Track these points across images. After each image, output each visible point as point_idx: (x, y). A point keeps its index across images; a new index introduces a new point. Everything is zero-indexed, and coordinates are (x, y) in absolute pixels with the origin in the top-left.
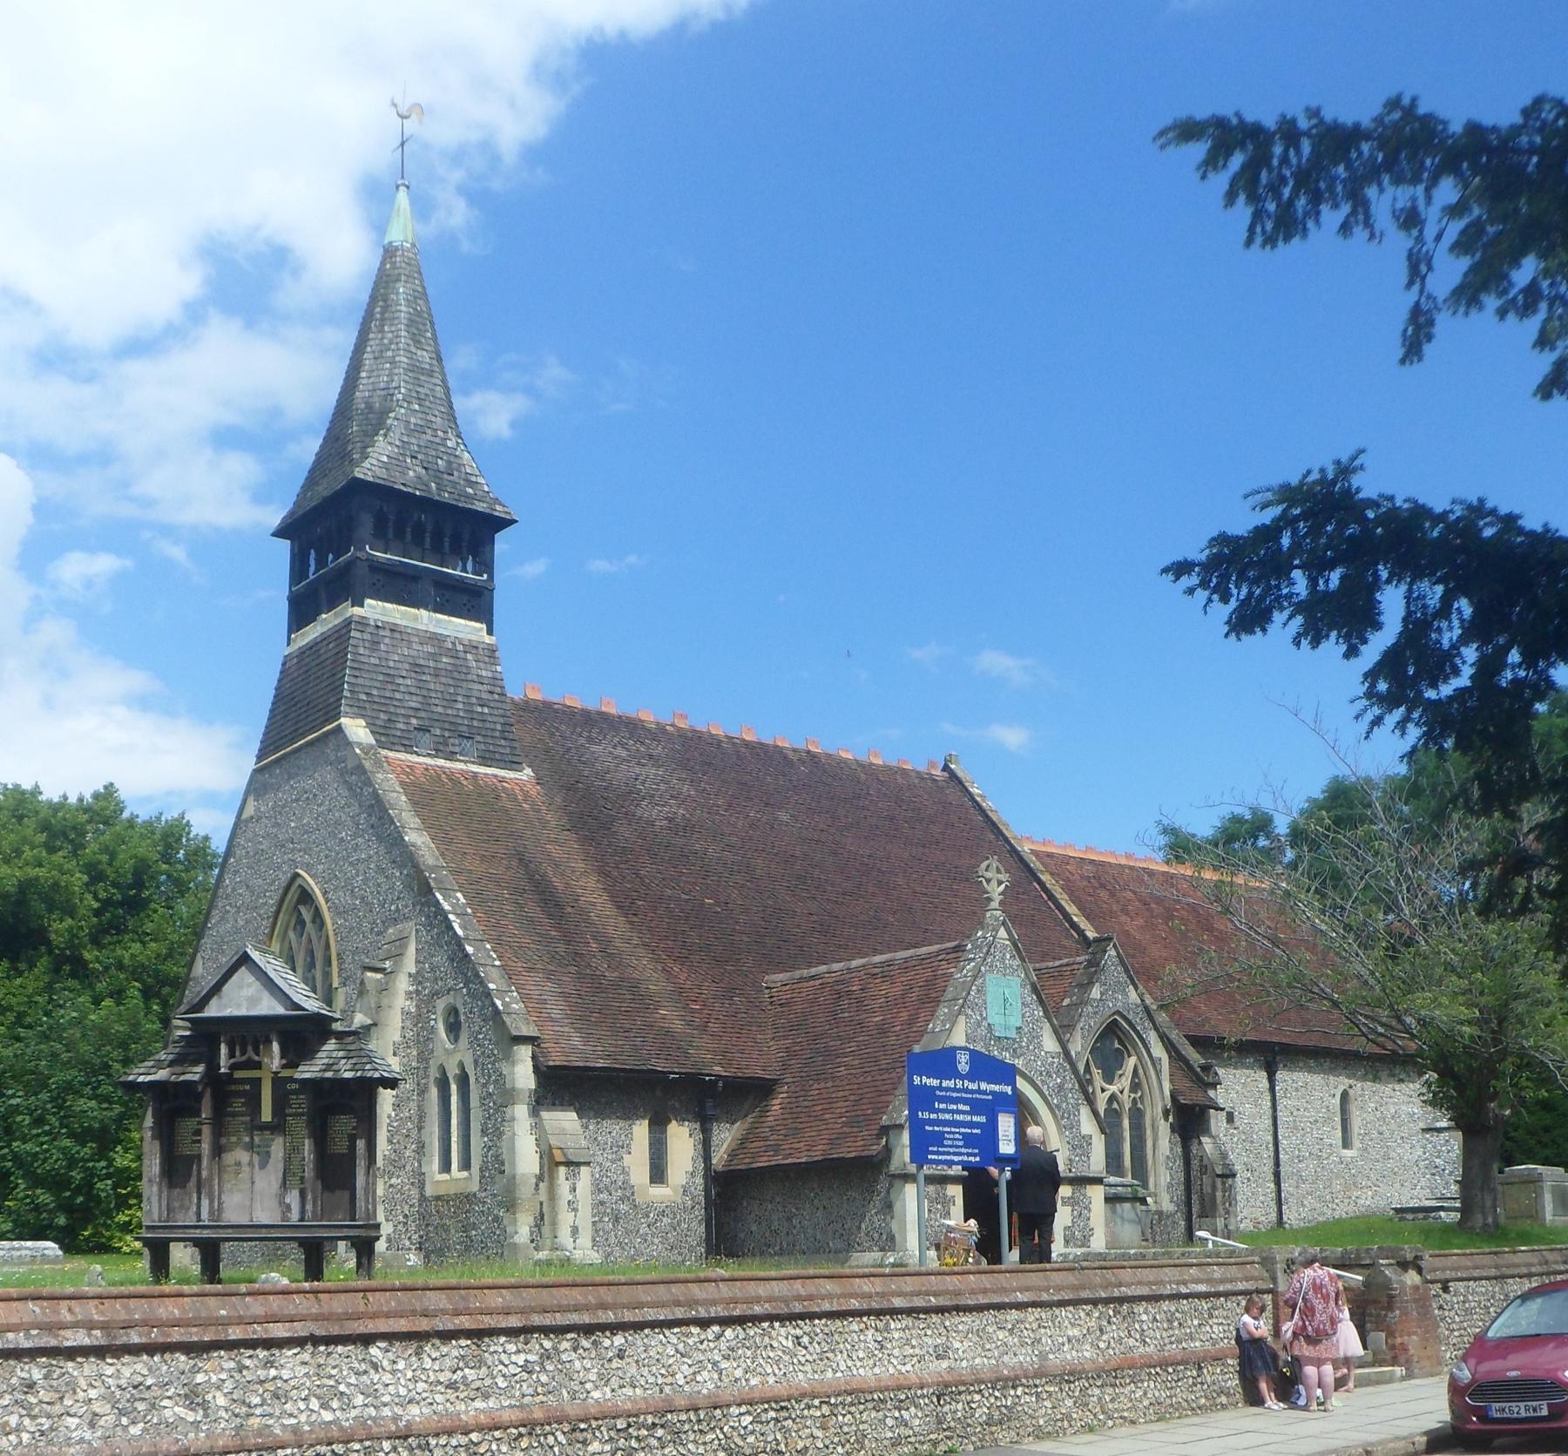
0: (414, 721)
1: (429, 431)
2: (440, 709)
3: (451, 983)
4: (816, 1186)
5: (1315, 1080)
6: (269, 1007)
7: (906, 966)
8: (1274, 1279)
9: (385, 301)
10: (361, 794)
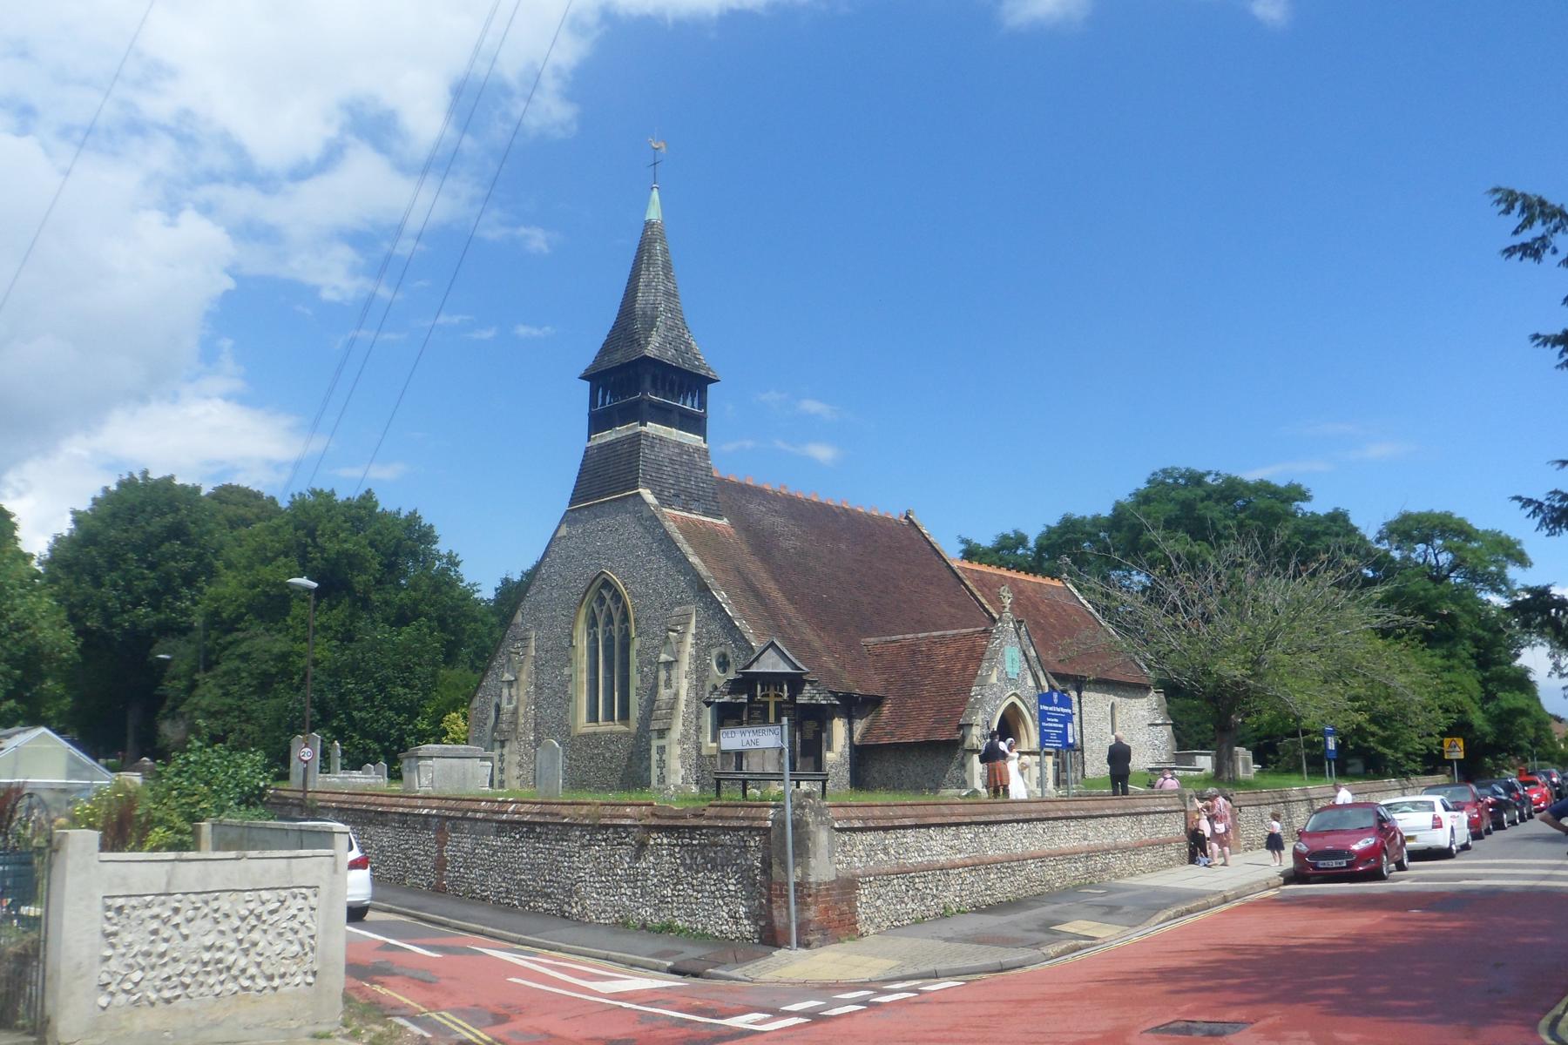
2: (683, 485)
5: (1099, 696)
7: (954, 638)
8: (1185, 805)
10: (654, 533)
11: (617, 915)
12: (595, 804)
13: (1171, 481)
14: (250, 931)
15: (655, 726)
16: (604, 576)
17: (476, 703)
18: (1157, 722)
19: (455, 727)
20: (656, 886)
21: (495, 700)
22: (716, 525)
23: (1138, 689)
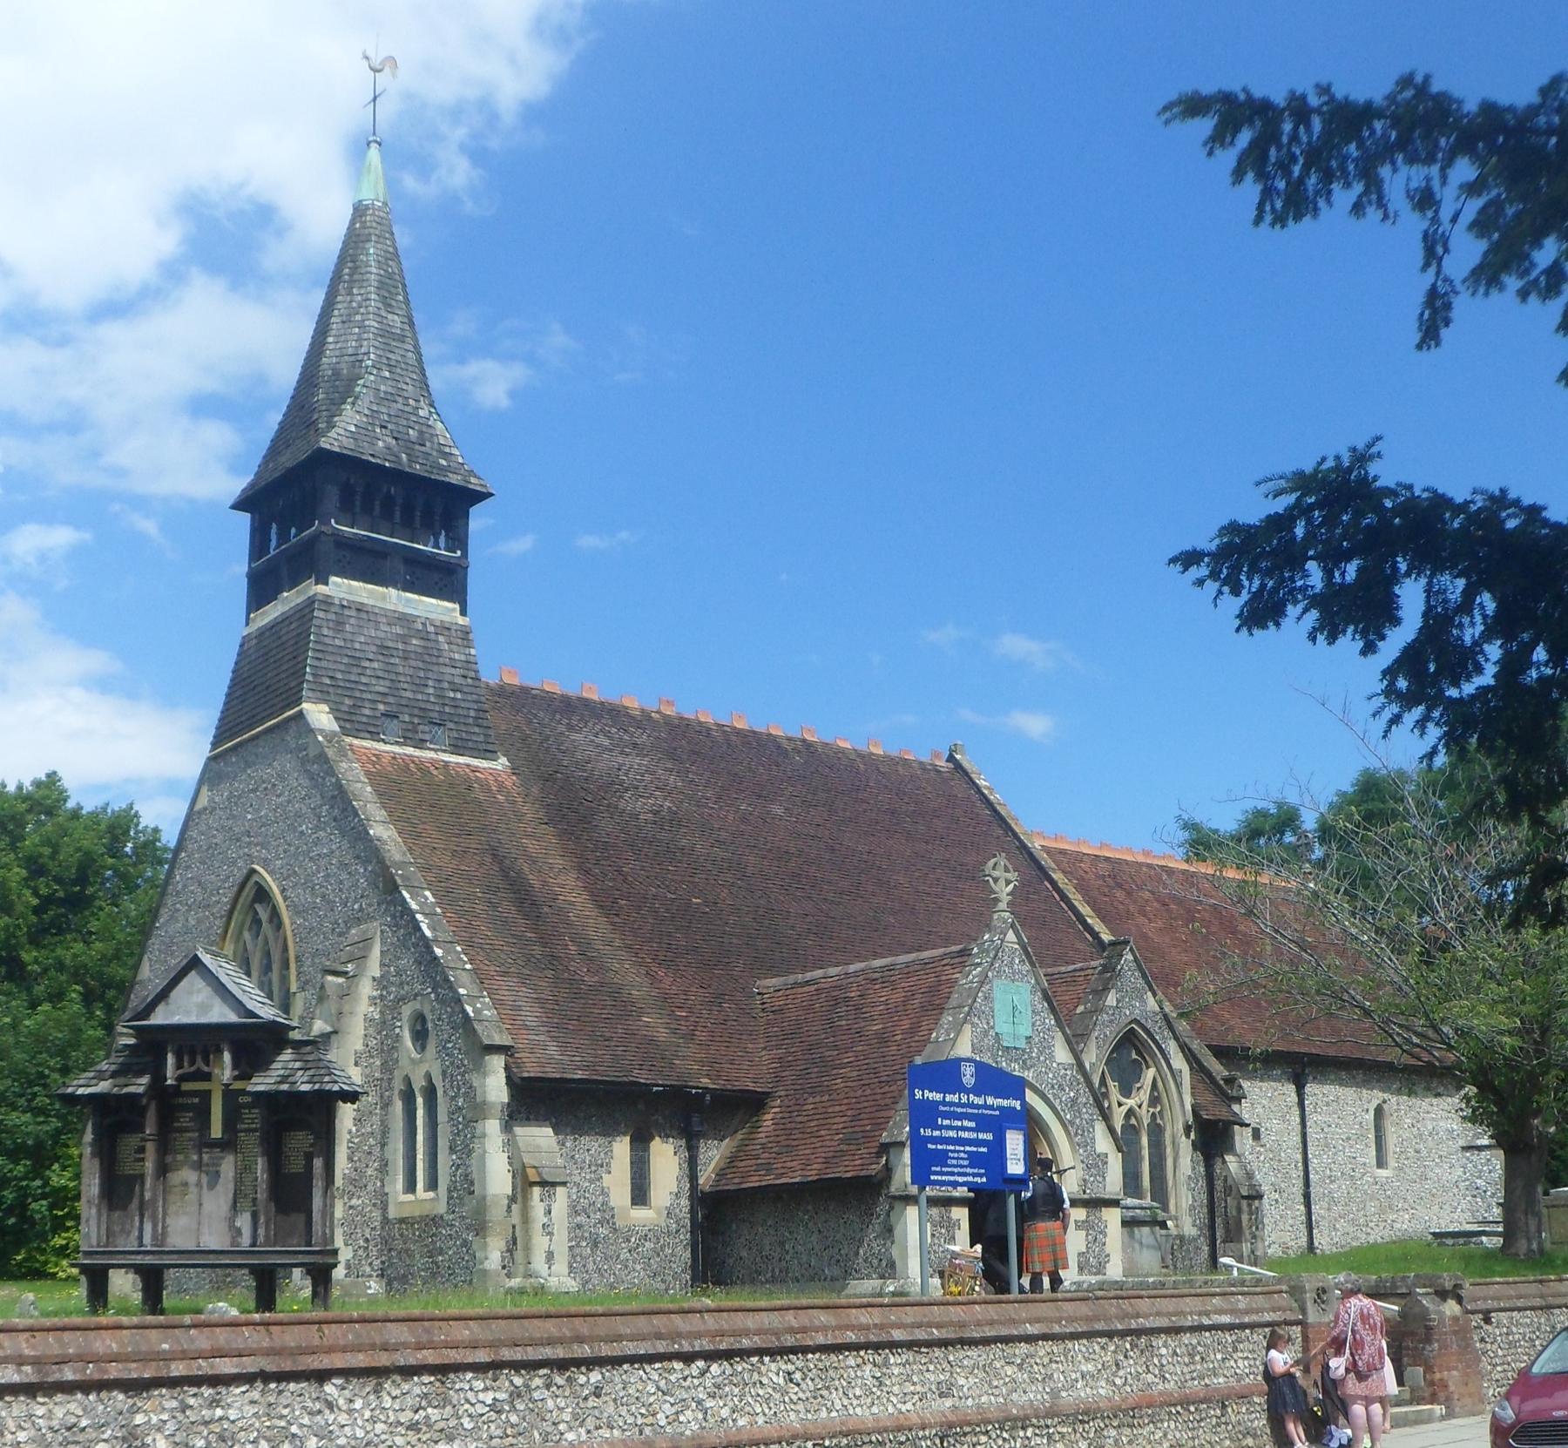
0: (381, 707)
1: (400, 400)
2: (409, 694)
4: (810, 1208)
5: (1348, 1094)
6: (221, 1014)
7: (908, 971)
8: (1303, 1310)
18: (1479, 1142)
22: (475, 770)
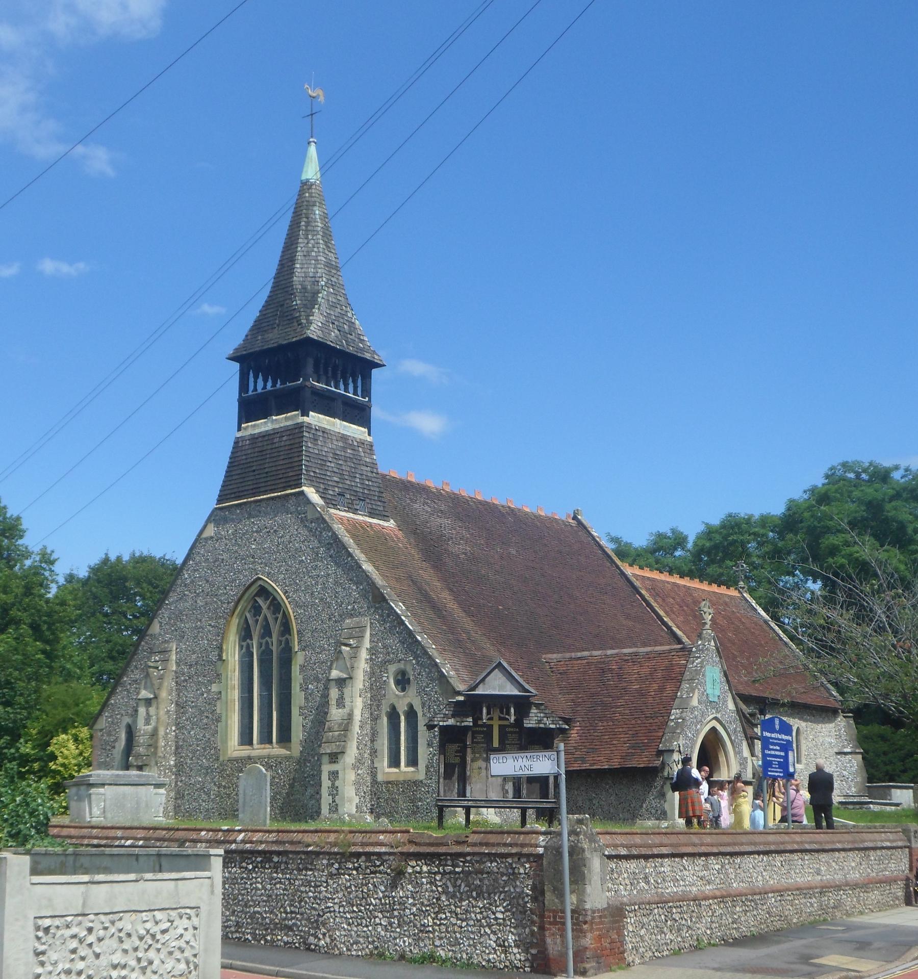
0: (336, 489)
1: (338, 306)
2: (348, 482)
3: (401, 656)
4: (610, 782)
6: (511, 690)
7: (648, 657)
8: (910, 841)
9: (308, 218)
10: (320, 536)
11: (371, 946)
12: (343, 831)
13: (852, 475)
14: (146, 950)
15: (327, 749)
16: (260, 583)
17: (102, 723)
18: (846, 750)
19: (66, 752)
20: (415, 916)
21: (127, 720)
23: (824, 713)
